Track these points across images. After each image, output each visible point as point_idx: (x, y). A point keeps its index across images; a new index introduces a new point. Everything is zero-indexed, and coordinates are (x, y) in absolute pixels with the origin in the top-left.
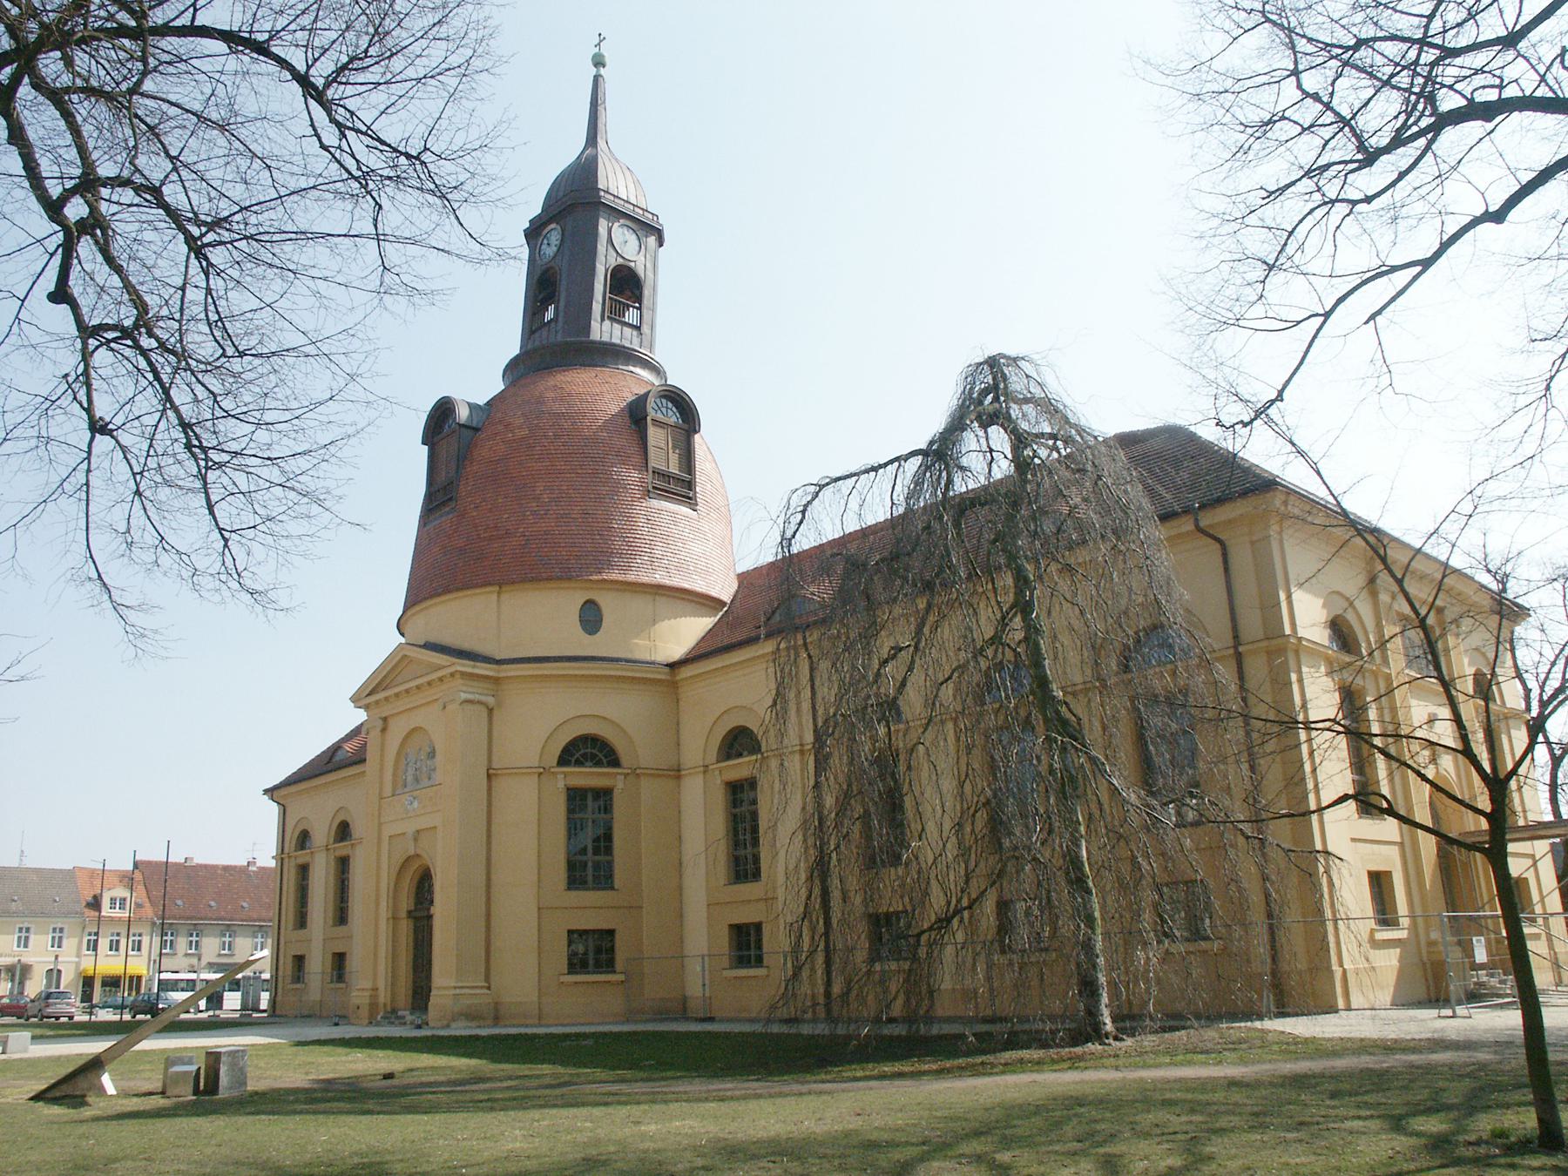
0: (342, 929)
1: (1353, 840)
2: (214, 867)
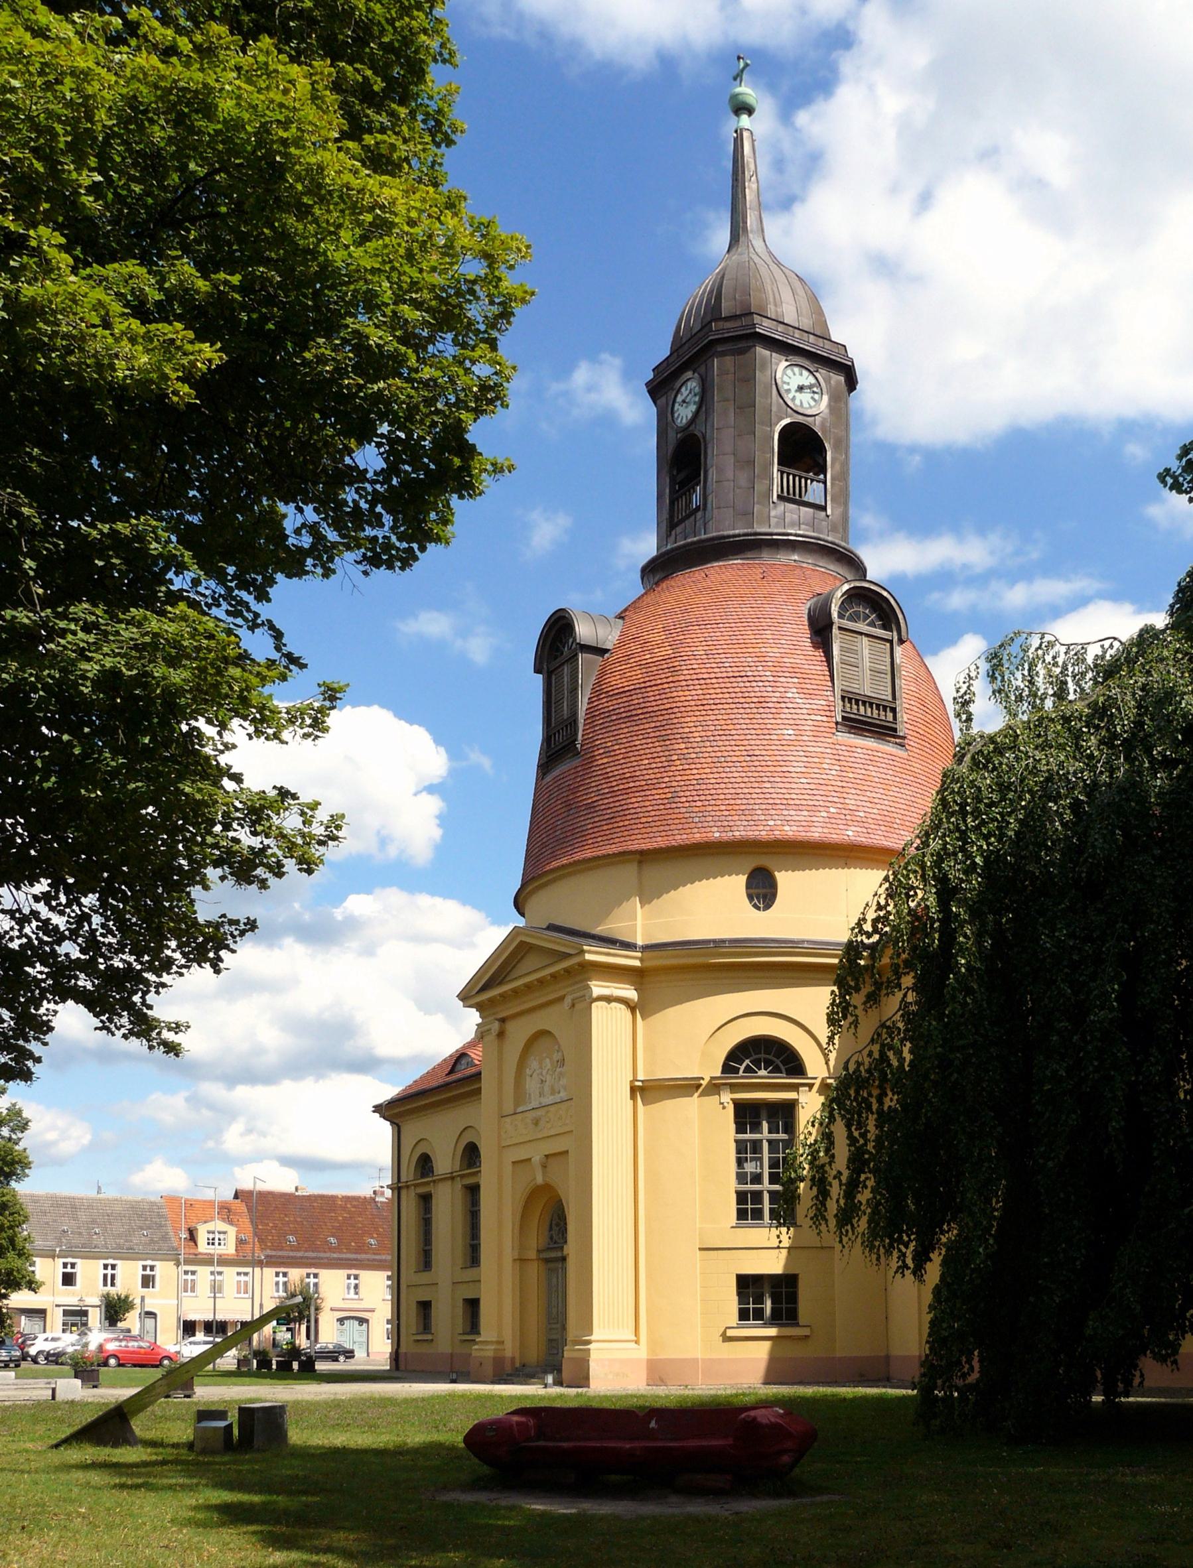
0: (470, 1274)
1: (700, 1249)
2: (333, 1198)
